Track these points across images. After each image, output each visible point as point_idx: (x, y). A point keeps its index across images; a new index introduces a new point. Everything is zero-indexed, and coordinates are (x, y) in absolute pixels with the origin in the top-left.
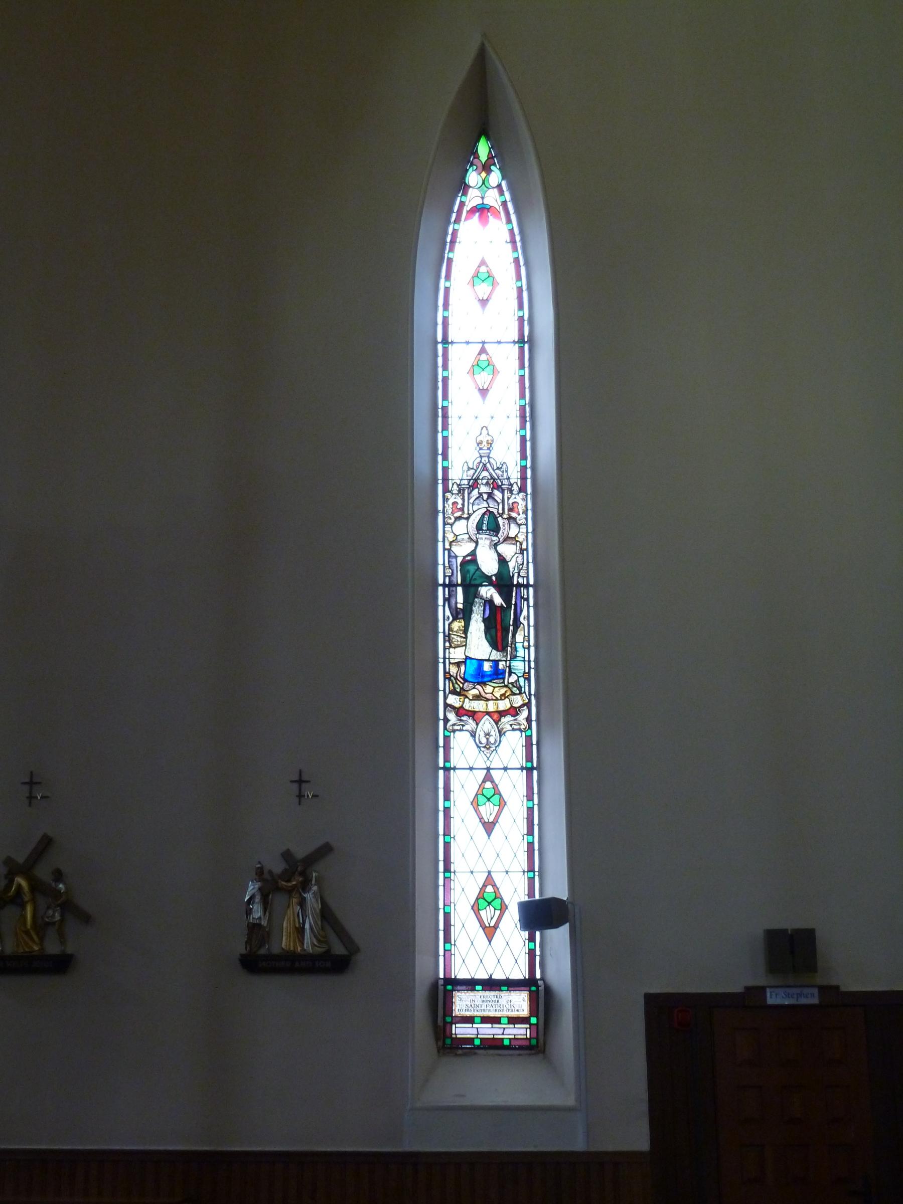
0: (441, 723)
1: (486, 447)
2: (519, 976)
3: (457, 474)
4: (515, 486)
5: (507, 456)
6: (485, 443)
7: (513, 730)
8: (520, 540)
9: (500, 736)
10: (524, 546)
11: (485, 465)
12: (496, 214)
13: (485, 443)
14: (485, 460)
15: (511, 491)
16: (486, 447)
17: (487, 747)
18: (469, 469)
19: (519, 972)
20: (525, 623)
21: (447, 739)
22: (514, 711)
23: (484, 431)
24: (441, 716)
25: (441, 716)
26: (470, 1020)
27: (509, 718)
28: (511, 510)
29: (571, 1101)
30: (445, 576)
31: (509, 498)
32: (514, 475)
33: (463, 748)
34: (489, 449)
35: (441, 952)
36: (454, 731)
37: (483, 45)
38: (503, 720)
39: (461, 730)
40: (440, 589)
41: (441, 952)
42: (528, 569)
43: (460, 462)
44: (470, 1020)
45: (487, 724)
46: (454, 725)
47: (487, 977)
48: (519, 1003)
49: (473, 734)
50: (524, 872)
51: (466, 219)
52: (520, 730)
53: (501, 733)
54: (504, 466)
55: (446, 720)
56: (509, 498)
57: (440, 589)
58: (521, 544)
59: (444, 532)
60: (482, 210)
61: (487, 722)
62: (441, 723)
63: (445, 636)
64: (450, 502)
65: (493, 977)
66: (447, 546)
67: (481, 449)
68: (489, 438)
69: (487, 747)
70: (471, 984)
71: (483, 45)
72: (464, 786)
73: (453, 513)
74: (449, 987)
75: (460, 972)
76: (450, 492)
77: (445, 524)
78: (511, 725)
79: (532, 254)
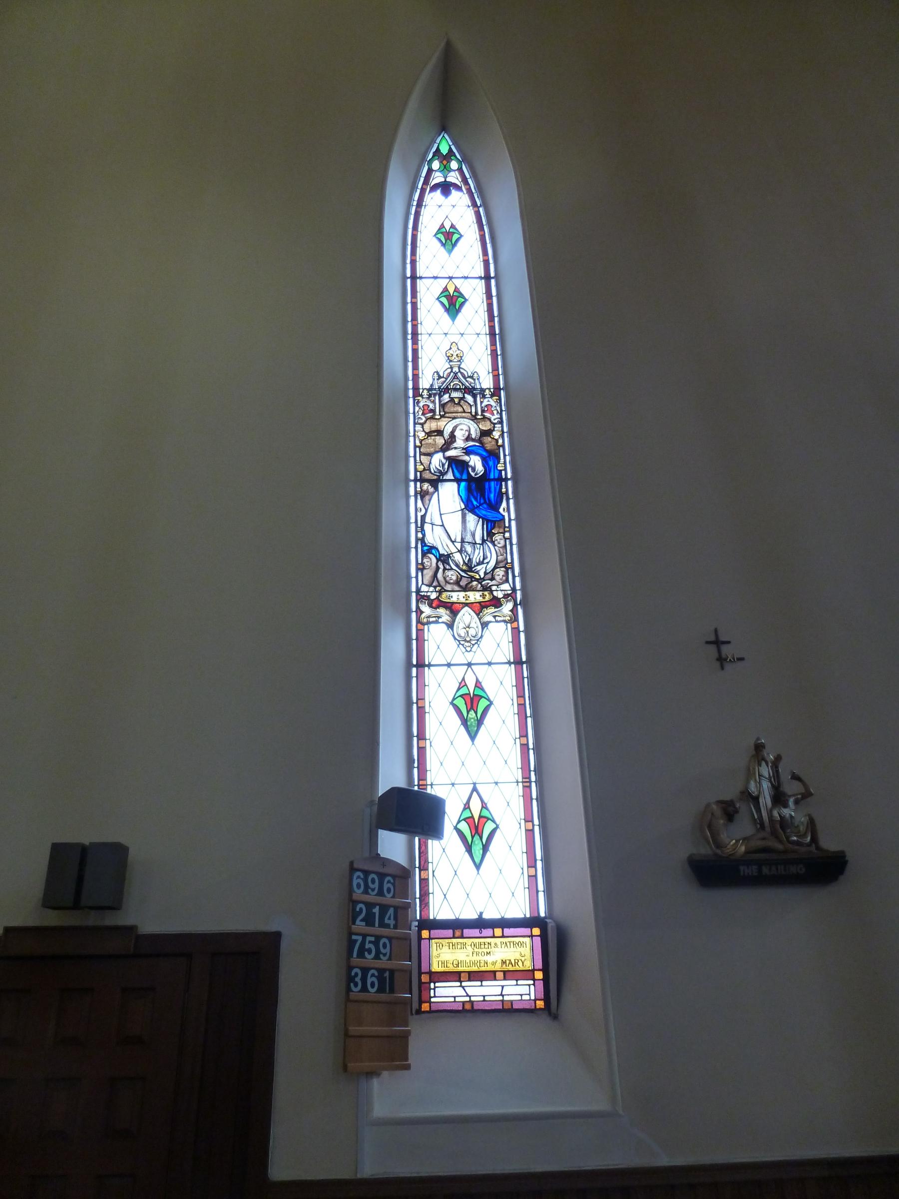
0: (414, 615)
1: (454, 358)
2: (520, 915)
3: (425, 382)
4: (487, 391)
5: (479, 365)
6: (455, 356)
7: (497, 621)
8: (496, 437)
9: (483, 629)
10: (500, 442)
11: (456, 374)
12: (458, 188)
13: (455, 356)
14: (456, 369)
15: (484, 397)
16: (454, 358)
17: (468, 642)
18: (440, 377)
19: (519, 909)
20: (506, 514)
21: (420, 632)
22: (496, 603)
23: (454, 348)
24: (414, 608)
25: (414, 608)
26: (455, 976)
27: (492, 610)
28: (483, 411)
29: (601, 1105)
30: (416, 470)
31: (481, 402)
32: (487, 382)
33: (439, 641)
34: (459, 361)
35: (539, 865)
36: (428, 623)
37: (449, 46)
38: (486, 611)
39: (437, 622)
40: (412, 484)
41: (539, 865)
42: (505, 463)
43: (432, 366)
44: (455, 976)
45: (466, 616)
46: (429, 617)
47: (475, 916)
48: (520, 951)
49: (450, 626)
50: (517, 782)
51: (430, 192)
52: (504, 621)
53: (485, 625)
54: (476, 375)
55: (419, 612)
56: (481, 402)
57: (412, 484)
58: (497, 441)
59: (415, 431)
60: (446, 188)
61: (467, 614)
62: (414, 615)
63: (417, 527)
64: (421, 404)
65: (485, 916)
66: (418, 443)
67: (451, 361)
68: (458, 352)
69: (468, 642)
70: (457, 928)
71: (449, 46)
72: (439, 690)
73: (423, 414)
74: (425, 934)
75: (439, 910)
76: (421, 396)
77: (415, 424)
78: (495, 617)
79: (497, 215)
